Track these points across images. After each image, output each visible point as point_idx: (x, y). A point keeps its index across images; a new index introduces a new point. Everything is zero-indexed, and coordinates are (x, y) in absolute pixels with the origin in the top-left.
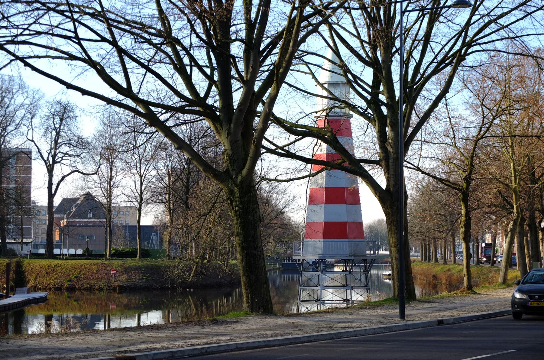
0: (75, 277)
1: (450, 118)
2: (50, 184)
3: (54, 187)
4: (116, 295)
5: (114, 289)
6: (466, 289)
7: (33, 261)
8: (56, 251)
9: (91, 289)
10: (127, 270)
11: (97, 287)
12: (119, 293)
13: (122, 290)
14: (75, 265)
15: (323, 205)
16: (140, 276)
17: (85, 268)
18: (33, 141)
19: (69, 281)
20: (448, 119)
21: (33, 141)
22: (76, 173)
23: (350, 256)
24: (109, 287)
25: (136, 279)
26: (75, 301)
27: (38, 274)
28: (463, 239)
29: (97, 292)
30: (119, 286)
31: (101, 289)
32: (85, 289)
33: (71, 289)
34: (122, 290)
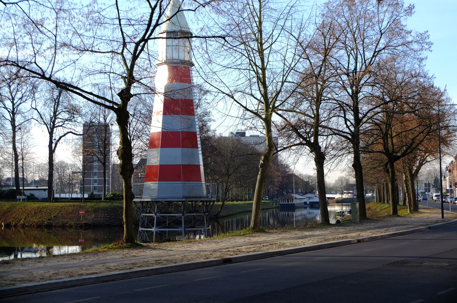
0: (54, 217)
1: (120, 20)
2: (51, 142)
3: (53, 145)
4: (84, 231)
5: (81, 227)
6: (125, 241)
7: (29, 203)
8: (57, 196)
9: (63, 226)
10: (96, 211)
11: (68, 225)
12: (85, 230)
13: (87, 227)
14: (58, 206)
15: (159, 149)
16: (104, 216)
17: (64, 209)
18: (36, 109)
19: (49, 219)
20: (117, 22)
21: (36, 109)
22: (70, 133)
23: (183, 198)
24: (78, 224)
25: (91, 218)
26: (54, 236)
27: (28, 214)
28: (121, 174)
29: (68, 228)
30: (85, 224)
31: (71, 227)
32: (59, 227)
33: (49, 226)
34: (87, 227)
